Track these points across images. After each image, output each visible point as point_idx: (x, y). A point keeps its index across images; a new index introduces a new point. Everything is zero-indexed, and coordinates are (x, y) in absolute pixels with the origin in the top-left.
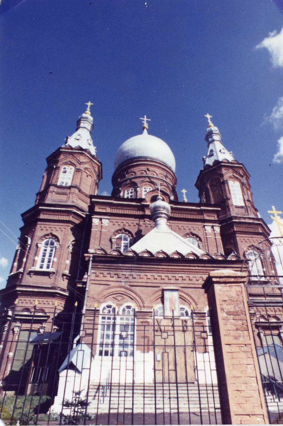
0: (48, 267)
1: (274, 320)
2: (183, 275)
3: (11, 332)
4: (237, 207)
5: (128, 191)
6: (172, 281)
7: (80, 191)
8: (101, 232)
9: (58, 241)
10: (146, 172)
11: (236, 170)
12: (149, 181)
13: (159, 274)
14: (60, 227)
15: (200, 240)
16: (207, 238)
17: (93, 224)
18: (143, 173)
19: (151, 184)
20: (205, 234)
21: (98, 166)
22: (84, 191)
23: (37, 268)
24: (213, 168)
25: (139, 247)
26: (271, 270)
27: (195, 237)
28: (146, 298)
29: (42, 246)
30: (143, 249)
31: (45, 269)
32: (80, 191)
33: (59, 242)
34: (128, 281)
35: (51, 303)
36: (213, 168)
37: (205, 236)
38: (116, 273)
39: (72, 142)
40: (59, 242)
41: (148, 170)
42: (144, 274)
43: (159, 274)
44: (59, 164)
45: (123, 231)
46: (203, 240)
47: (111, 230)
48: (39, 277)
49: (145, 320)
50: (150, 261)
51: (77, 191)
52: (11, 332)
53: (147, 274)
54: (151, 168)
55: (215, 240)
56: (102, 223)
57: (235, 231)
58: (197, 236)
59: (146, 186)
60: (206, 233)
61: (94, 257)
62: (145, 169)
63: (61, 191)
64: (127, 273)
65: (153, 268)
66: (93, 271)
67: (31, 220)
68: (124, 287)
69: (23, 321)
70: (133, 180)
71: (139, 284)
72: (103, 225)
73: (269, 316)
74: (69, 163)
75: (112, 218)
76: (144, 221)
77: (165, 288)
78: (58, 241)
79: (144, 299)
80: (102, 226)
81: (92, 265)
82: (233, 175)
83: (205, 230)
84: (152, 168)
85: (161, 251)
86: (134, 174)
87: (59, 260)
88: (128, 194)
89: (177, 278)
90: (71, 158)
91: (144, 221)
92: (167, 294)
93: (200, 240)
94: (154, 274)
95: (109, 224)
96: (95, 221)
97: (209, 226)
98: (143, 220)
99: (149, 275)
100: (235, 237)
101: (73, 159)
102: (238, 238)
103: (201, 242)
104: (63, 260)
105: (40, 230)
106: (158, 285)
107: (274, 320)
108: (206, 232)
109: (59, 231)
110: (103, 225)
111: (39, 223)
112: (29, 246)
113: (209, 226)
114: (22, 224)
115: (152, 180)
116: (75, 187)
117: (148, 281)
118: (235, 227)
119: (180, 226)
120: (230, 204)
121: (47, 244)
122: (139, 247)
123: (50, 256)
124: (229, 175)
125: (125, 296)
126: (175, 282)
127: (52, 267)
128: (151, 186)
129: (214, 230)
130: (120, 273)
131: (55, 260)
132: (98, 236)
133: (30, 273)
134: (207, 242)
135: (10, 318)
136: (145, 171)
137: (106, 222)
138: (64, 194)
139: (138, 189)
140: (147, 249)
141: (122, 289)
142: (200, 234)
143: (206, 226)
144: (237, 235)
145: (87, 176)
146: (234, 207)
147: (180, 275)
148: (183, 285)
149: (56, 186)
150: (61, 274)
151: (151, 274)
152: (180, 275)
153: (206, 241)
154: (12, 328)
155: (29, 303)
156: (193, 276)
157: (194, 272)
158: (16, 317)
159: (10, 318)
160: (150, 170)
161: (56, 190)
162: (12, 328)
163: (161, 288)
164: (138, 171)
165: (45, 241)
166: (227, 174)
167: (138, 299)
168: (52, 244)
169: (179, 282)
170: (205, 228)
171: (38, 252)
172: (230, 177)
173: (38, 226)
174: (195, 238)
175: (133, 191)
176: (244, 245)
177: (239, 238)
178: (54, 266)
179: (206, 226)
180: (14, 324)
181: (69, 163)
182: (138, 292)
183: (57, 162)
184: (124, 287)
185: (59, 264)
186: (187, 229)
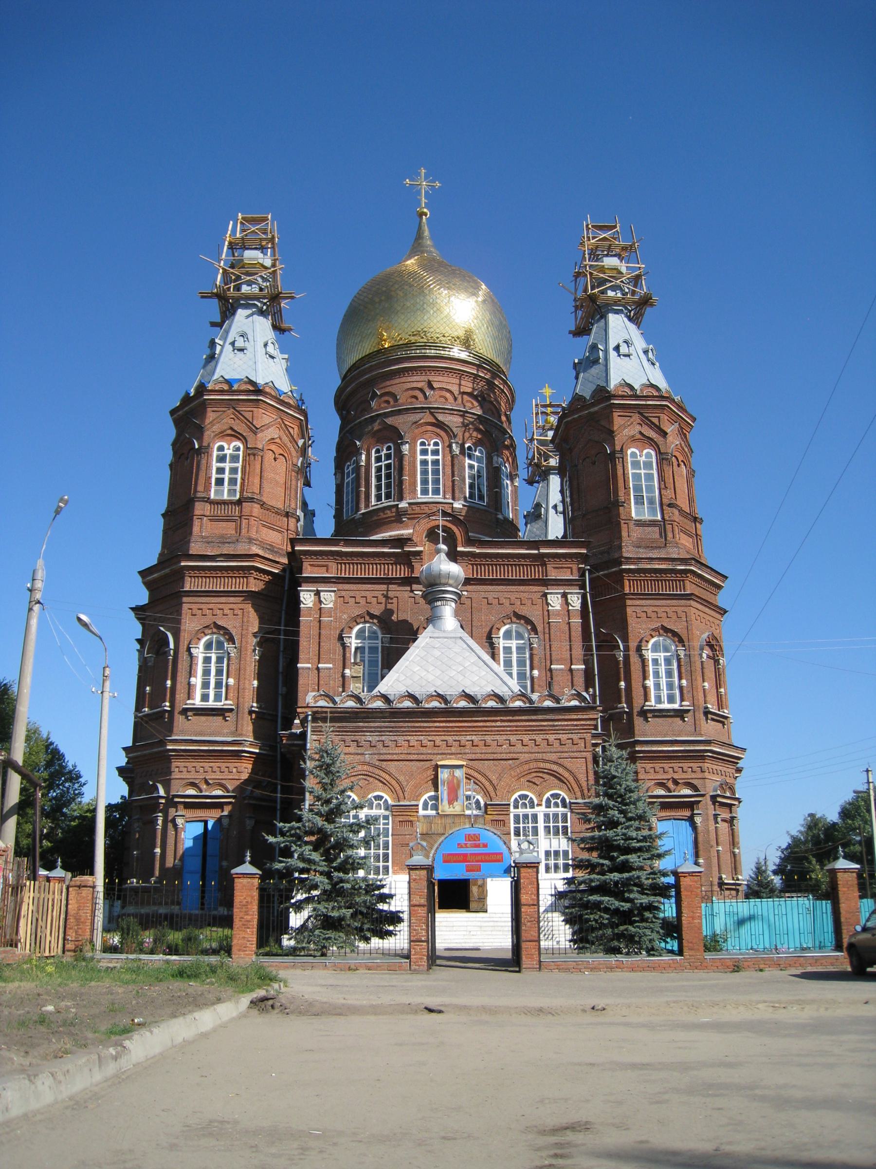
0: (218, 698)
1: (687, 791)
2: (473, 737)
3: (170, 825)
4: (640, 523)
5: (378, 451)
6: (453, 750)
7: (263, 505)
8: (320, 621)
9: (231, 640)
10: (425, 394)
11: (646, 415)
12: (434, 421)
13: (430, 738)
14: (232, 606)
15: (534, 630)
16: (549, 623)
17: (302, 606)
18: (416, 398)
19: (438, 431)
20: (546, 613)
21: (298, 422)
22: (272, 503)
23: (197, 701)
24: (592, 410)
25: (398, 682)
26: (700, 679)
27: (522, 622)
28: (407, 781)
29: (199, 652)
30: (402, 689)
31: (211, 703)
32: (263, 505)
33: (234, 644)
34: (376, 752)
35: (234, 770)
36: (592, 410)
37: (546, 618)
38: (354, 738)
39: (230, 366)
40: (234, 644)
41: (430, 386)
42: (403, 738)
43: (430, 738)
44: (208, 434)
45: (367, 618)
46: (540, 629)
47: (340, 617)
48: (203, 718)
49: (407, 818)
50: (416, 714)
51: (256, 509)
52: (170, 825)
53: (409, 738)
54: (434, 378)
55: (567, 628)
56: (320, 602)
57: (626, 594)
58: (528, 621)
59: (424, 436)
60: (548, 611)
61: (314, 713)
62: (419, 385)
63: (220, 511)
64: (373, 738)
65: (420, 727)
66: (315, 737)
67: (164, 593)
68: (369, 764)
69: (187, 806)
70: (389, 421)
71: (395, 757)
72: (323, 606)
73: (676, 782)
74: (229, 432)
75: (341, 586)
76: (412, 591)
77: (440, 763)
78: (231, 640)
79: (404, 784)
80: (320, 609)
81: (312, 727)
82: (641, 433)
83: (548, 604)
84: (440, 378)
85: (435, 694)
86: (391, 400)
87: (238, 680)
88: (378, 459)
89: (463, 743)
90: (233, 416)
91: (412, 591)
92: (444, 775)
93: (534, 630)
94: (422, 738)
95: (335, 602)
96: (307, 598)
97: (557, 593)
98: (409, 588)
99: (413, 740)
100: (625, 606)
101: (237, 421)
102: (629, 610)
103: (536, 633)
104: (247, 682)
105: (189, 616)
106: (429, 757)
107: (687, 791)
108: (550, 608)
109: (231, 616)
110: (323, 606)
111: (185, 599)
112: (172, 652)
113: (557, 593)
114: (142, 597)
115: (441, 417)
116: (251, 500)
117: (411, 750)
118: (626, 583)
119: (491, 596)
120: (622, 517)
121: (208, 646)
122: (398, 682)
123: (219, 672)
124: (632, 433)
125: (371, 779)
126: (459, 752)
127: (226, 699)
128: (438, 435)
129: (567, 604)
130: (361, 739)
131: (231, 681)
132: (314, 632)
133: (185, 712)
134: (549, 634)
135: (163, 801)
136: (421, 390)
137: (329, 598)
138: (228, 521)
139: (406, 448)
140: (410, 691)
141: (365, 767)
142: (535, 614)
143: (551, 593)
144: (629, 602)
145: (275, 459)
146: (631, 524)
147: (468, 738)
148: (473, 756)
149: (208, 500)
150: (246, 711)
151: (416, 738)
152: (468, 738)
153: (547, 630)
154: (170, 818)
155: (193, 772)
156: (492, 737)
157: (492, 731)
158: (176, 800)
159: (163, 801)
160: (435, 385)
161: (207, 509)
162: (170, 818)
163: (433, 763)
164: (401, 387)
165: (205, 639)
166: (626, 428)
167: (394, 782)
168: (220, 645)
169: (467, 751)
170: (547, 599)
171: (194, 666)
172: (633, 440)
173: (185, 607)
174: (522, 625)
175: (392, 451)
176: (644, 626)
177: (633, 608)
178: (231, 695)
179: (551, 593)
180: (172, 812)
181: (229, 432)
182: (393, 771)
183: (199, 431)
184: (369, 764)
185: (239, 688)
186: (506, 603)
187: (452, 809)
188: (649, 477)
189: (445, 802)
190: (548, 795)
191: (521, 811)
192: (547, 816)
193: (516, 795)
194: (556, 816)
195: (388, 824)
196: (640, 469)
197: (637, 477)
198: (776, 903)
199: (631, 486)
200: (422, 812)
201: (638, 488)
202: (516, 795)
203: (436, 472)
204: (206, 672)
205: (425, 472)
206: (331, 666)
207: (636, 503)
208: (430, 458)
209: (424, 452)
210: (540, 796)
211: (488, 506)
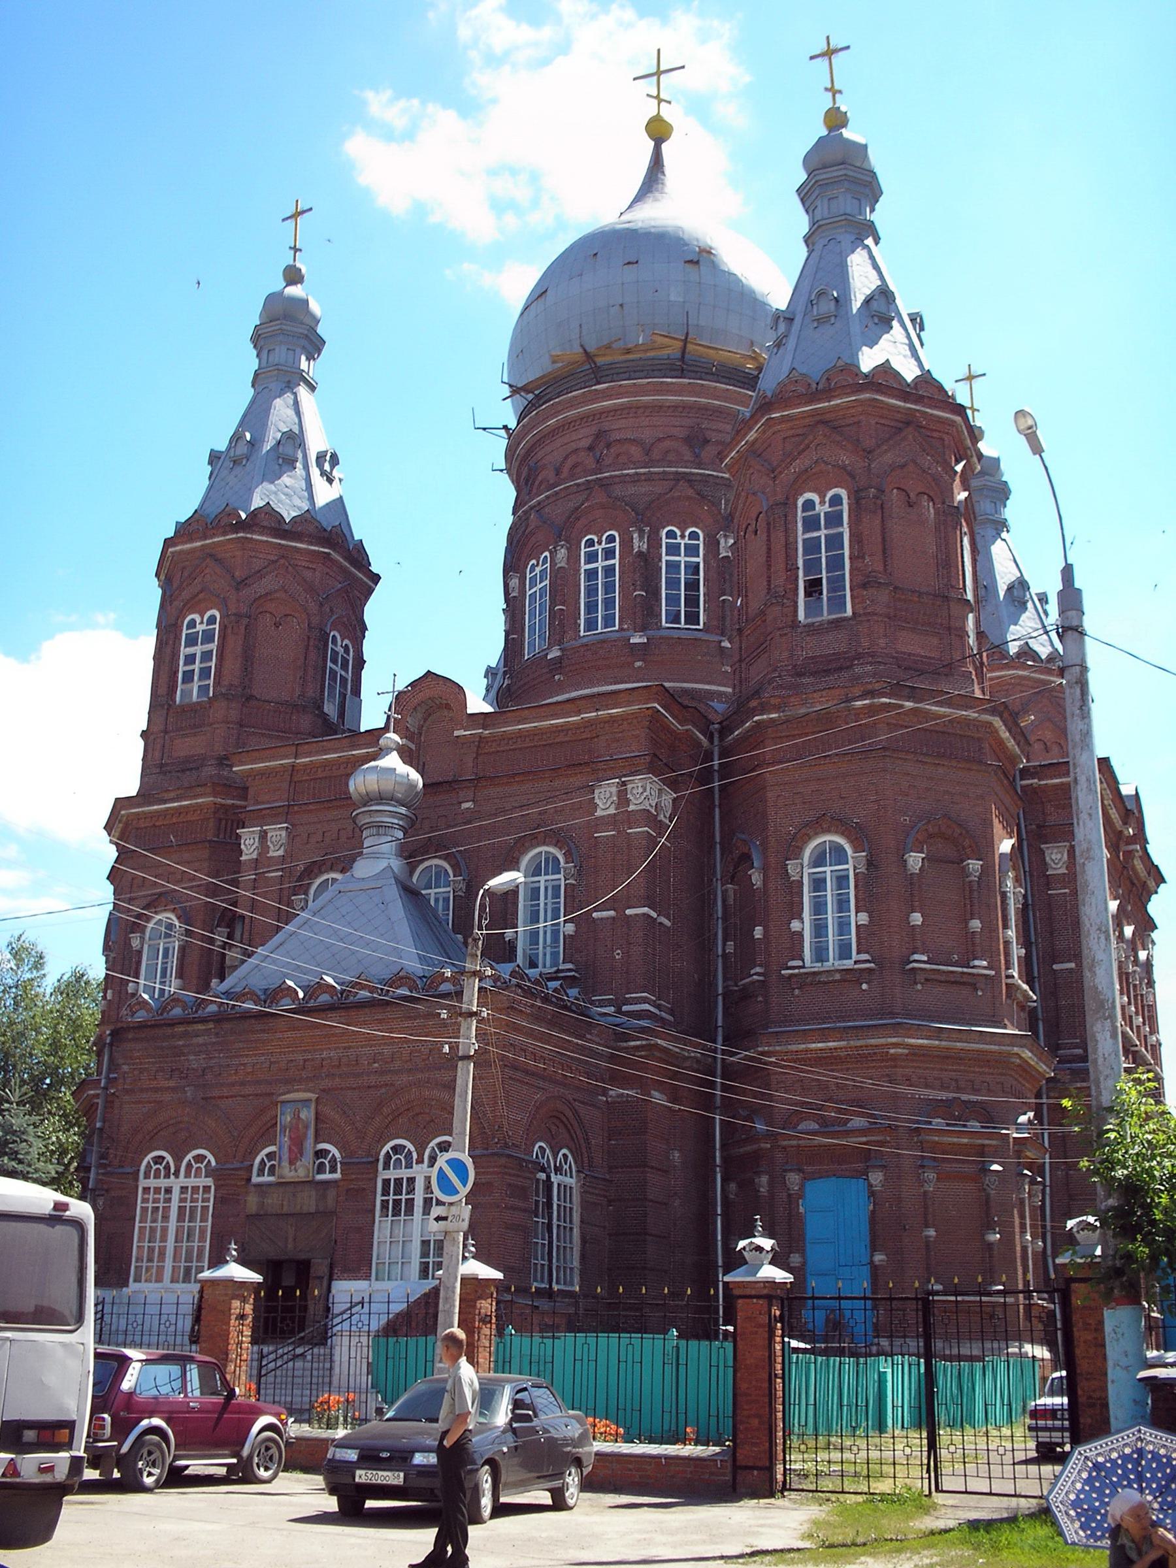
187: (293, 1173)
188: (834, 542)
189: (285, 1164)
190: (189, 1157)
191: (152, 1183)
192: (184, 1189)
193: (387, 1147)
194: (195, 1189)
195: (208, 1200)
196: (679, 555)
197: (673, 567)
198: (624, 1342)
199: (800, 563)
200: (255, 1179)
201: (812, 565)
202: (387, 1147)
203: (609, 588)
204: (819, 907)
205: (591, 591)
206: (628, 912)
207: (808, 594)
208: (682, 559)
209: (673, 550)
210: (178, 1159)
211: (706, 630)
